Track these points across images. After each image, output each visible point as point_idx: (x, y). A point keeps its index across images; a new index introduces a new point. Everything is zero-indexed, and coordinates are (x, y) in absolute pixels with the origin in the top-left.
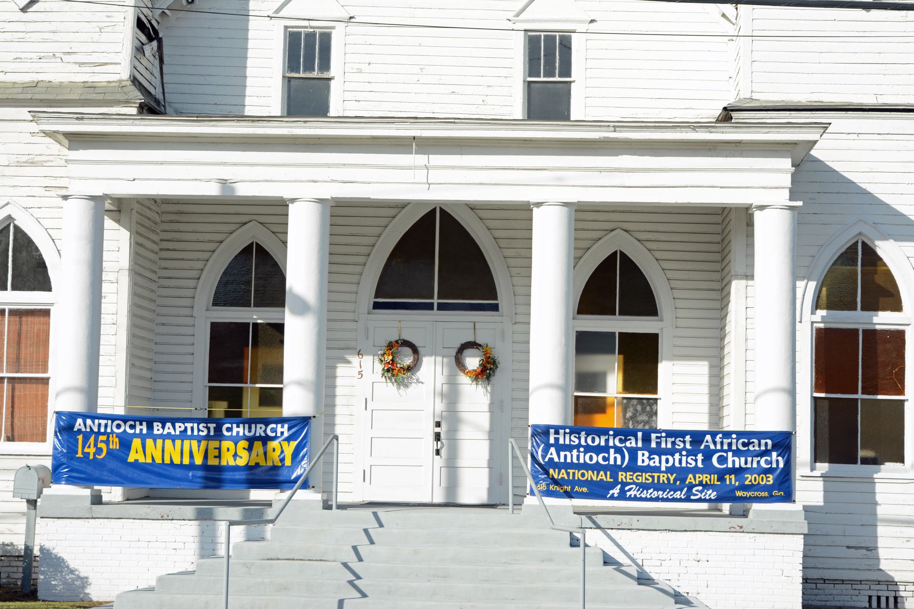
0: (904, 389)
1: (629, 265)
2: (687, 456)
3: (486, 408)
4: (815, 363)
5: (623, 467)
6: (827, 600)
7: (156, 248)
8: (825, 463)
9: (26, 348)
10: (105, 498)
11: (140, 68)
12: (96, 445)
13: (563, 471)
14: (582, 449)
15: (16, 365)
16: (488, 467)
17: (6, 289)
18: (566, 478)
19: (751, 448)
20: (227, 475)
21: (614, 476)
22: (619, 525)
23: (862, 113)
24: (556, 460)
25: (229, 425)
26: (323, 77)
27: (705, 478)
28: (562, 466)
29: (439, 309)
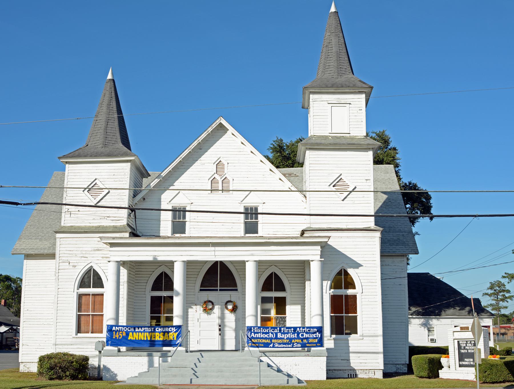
0: (357, 312)
1: (277, 277)
3: (234, 321)
7: (134, 274)
9: (97, 305)
10: (121, 350)
11: (130, 220)
12: (119, 335)
13: (256, 340)
14: (261, 333)
15: (94, 310)
17: (91, 288)
19: (311, 332)
20: (156, 343)
21: (271, 341)
24: (254, 336)
25: (158, 328)
29: (220, 291)
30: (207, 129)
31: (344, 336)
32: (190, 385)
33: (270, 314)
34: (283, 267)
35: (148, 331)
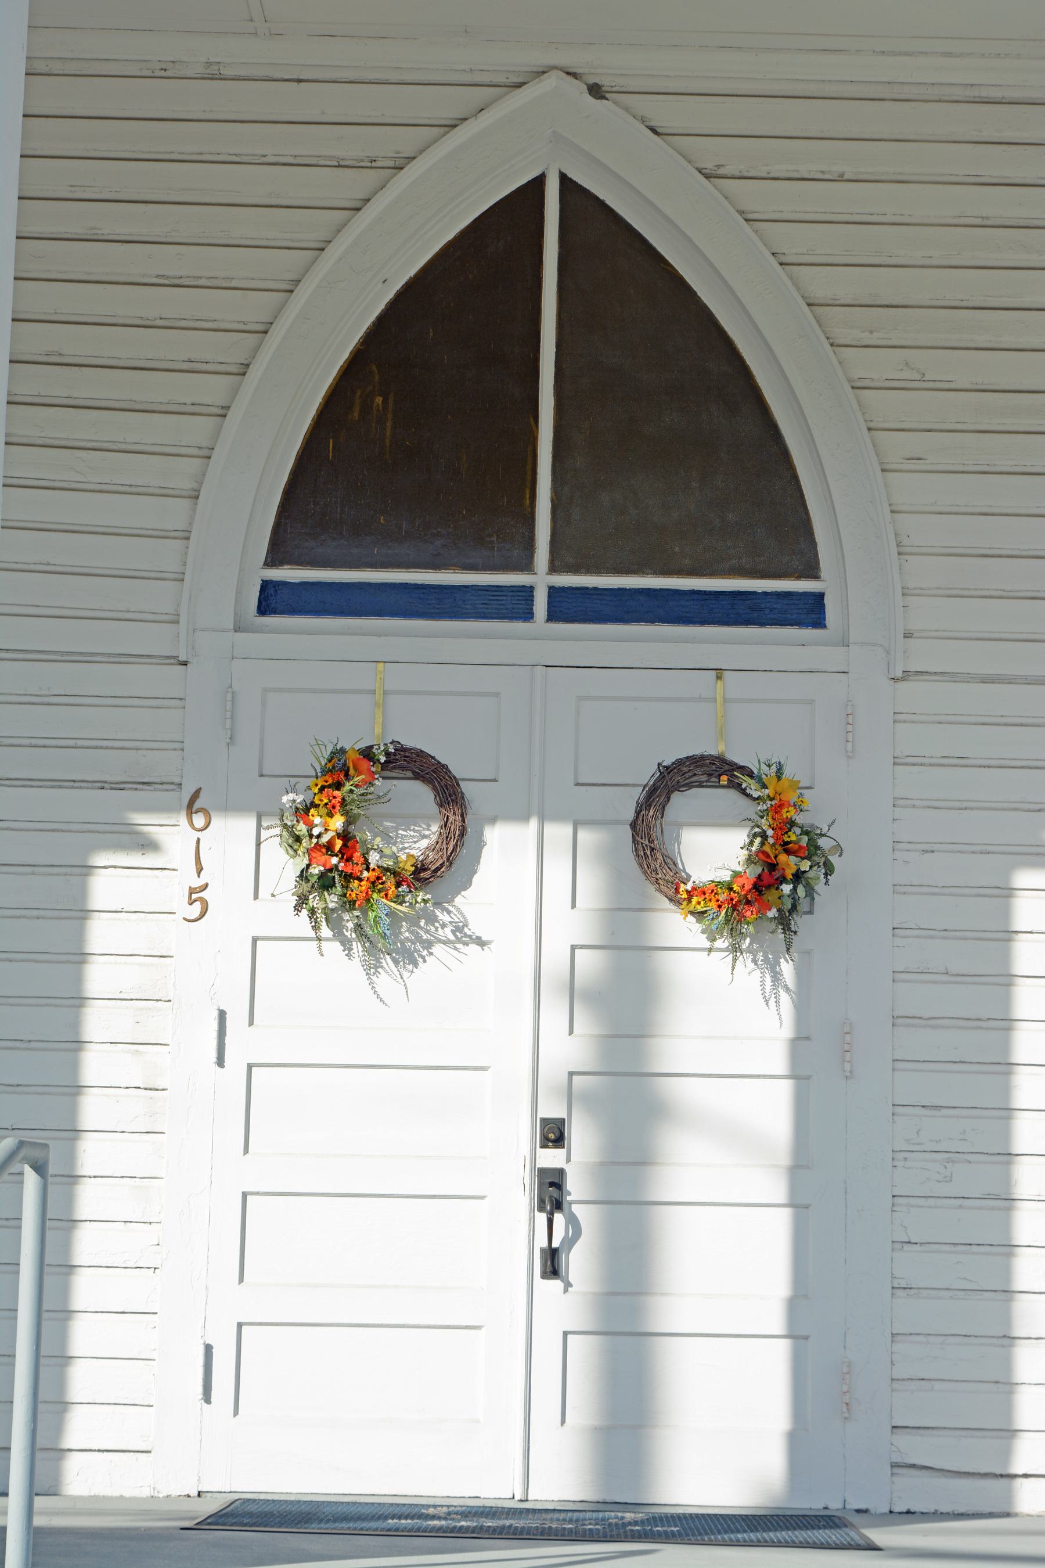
3: (778, 1061)
16: (790, 1205)
29: (553, 616)
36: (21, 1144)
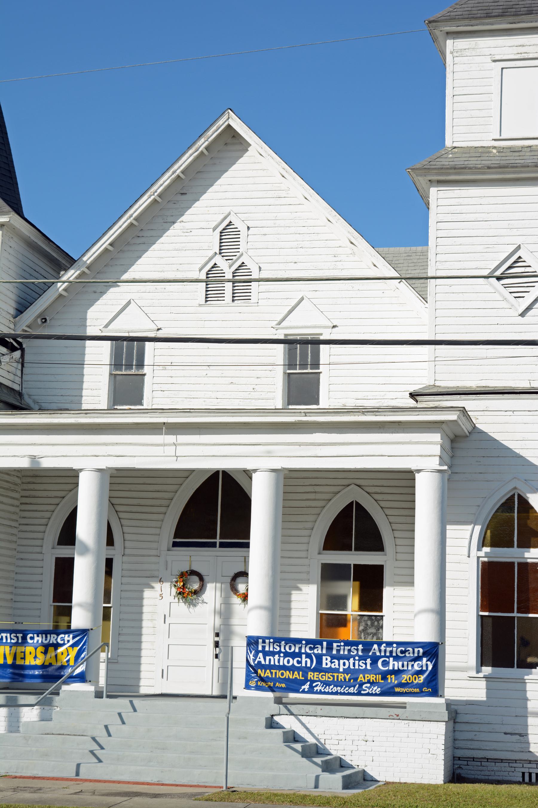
2: (359, 660)
4: (481, 589)
5: (312, 668)
6: (490, 775)
8: (489, 667)
13: (268, 671)
14: (282, 655)
18: (270, 676)
21: (305, 675)
22: (307, 713)
23: (515, 395)
24: (263, 662)
25: (32, 635)
26: (138, 373)
27: (372, 677)
28: (267, 667)
30: (194, 143)
31: (514, 672)
32: (76, 780)
33: (344, 607)
34: (378, 490)
35: (9, 641)
36: (104, 643)
